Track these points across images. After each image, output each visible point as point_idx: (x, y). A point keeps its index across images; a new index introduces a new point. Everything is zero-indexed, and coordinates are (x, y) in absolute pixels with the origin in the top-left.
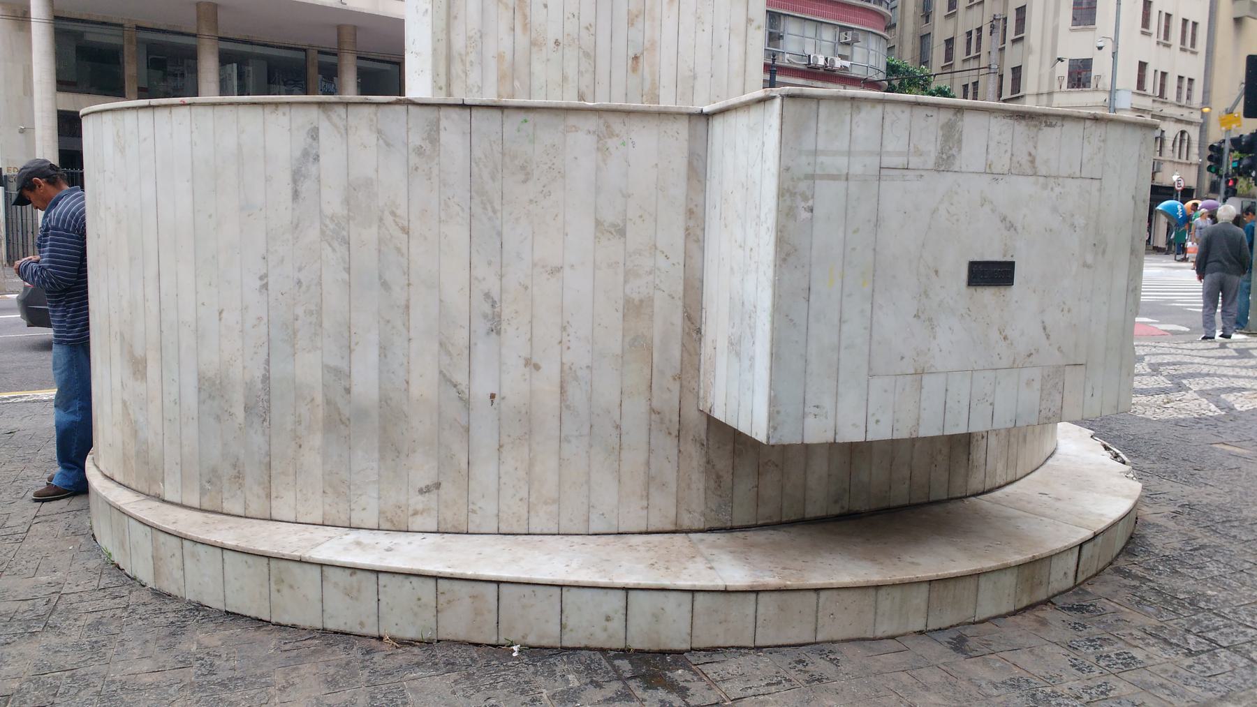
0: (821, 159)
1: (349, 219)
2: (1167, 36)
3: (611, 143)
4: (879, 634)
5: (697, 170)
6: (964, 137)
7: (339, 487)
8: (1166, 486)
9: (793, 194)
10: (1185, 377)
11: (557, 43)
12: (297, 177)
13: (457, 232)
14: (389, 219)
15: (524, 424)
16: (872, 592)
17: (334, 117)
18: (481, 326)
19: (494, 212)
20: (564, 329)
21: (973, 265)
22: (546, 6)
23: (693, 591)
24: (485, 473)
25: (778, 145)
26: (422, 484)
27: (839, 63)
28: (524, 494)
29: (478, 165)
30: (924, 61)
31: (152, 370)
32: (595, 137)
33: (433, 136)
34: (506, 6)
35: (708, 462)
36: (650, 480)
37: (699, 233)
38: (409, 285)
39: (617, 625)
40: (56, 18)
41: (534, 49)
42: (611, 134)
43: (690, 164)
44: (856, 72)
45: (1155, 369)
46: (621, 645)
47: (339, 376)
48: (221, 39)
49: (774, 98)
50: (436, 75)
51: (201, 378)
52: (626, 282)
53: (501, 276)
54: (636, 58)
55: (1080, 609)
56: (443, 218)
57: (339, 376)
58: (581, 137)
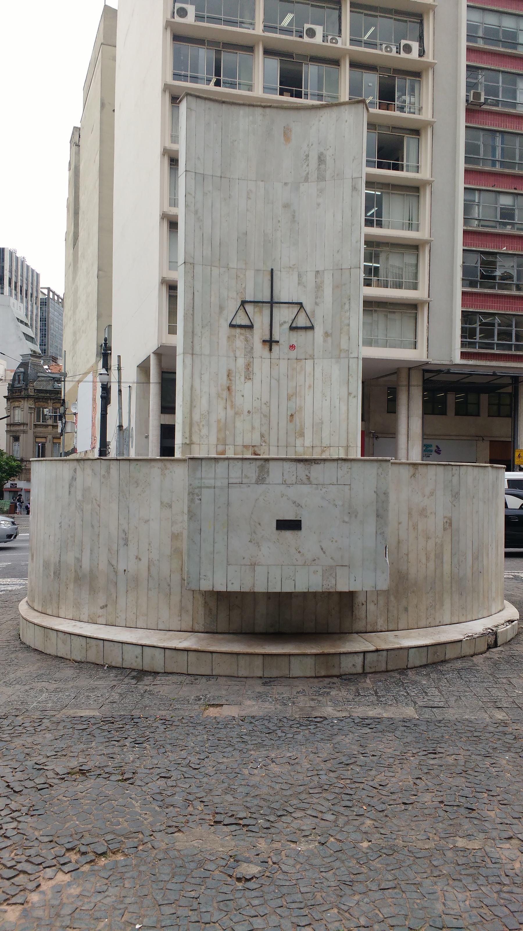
0: (203, 481)
3: (166, 472)
4: (240, 675)
6: (270, 470)
7: (77, 605)
9: (193, 494)
11: (249, 412)
12: (70, 486)
13: (114, 506)
14: (94, 501)
15: (135, 582)
16: (235, 656)
18: (121, 542)
19: (127, 499)
20: (150, 544)
22: (243, 396)
23: (165, 648)
24: (122, 601)
26: (102, 605)
34: (222, 398)
35: (205, 603)
36: (181, 608)
39: (139, 660)
40: (163, 372)
42: (166, 469)
46: (141, 669)
47: (79, 560)
52: (172, 526)
54: (292, 415)
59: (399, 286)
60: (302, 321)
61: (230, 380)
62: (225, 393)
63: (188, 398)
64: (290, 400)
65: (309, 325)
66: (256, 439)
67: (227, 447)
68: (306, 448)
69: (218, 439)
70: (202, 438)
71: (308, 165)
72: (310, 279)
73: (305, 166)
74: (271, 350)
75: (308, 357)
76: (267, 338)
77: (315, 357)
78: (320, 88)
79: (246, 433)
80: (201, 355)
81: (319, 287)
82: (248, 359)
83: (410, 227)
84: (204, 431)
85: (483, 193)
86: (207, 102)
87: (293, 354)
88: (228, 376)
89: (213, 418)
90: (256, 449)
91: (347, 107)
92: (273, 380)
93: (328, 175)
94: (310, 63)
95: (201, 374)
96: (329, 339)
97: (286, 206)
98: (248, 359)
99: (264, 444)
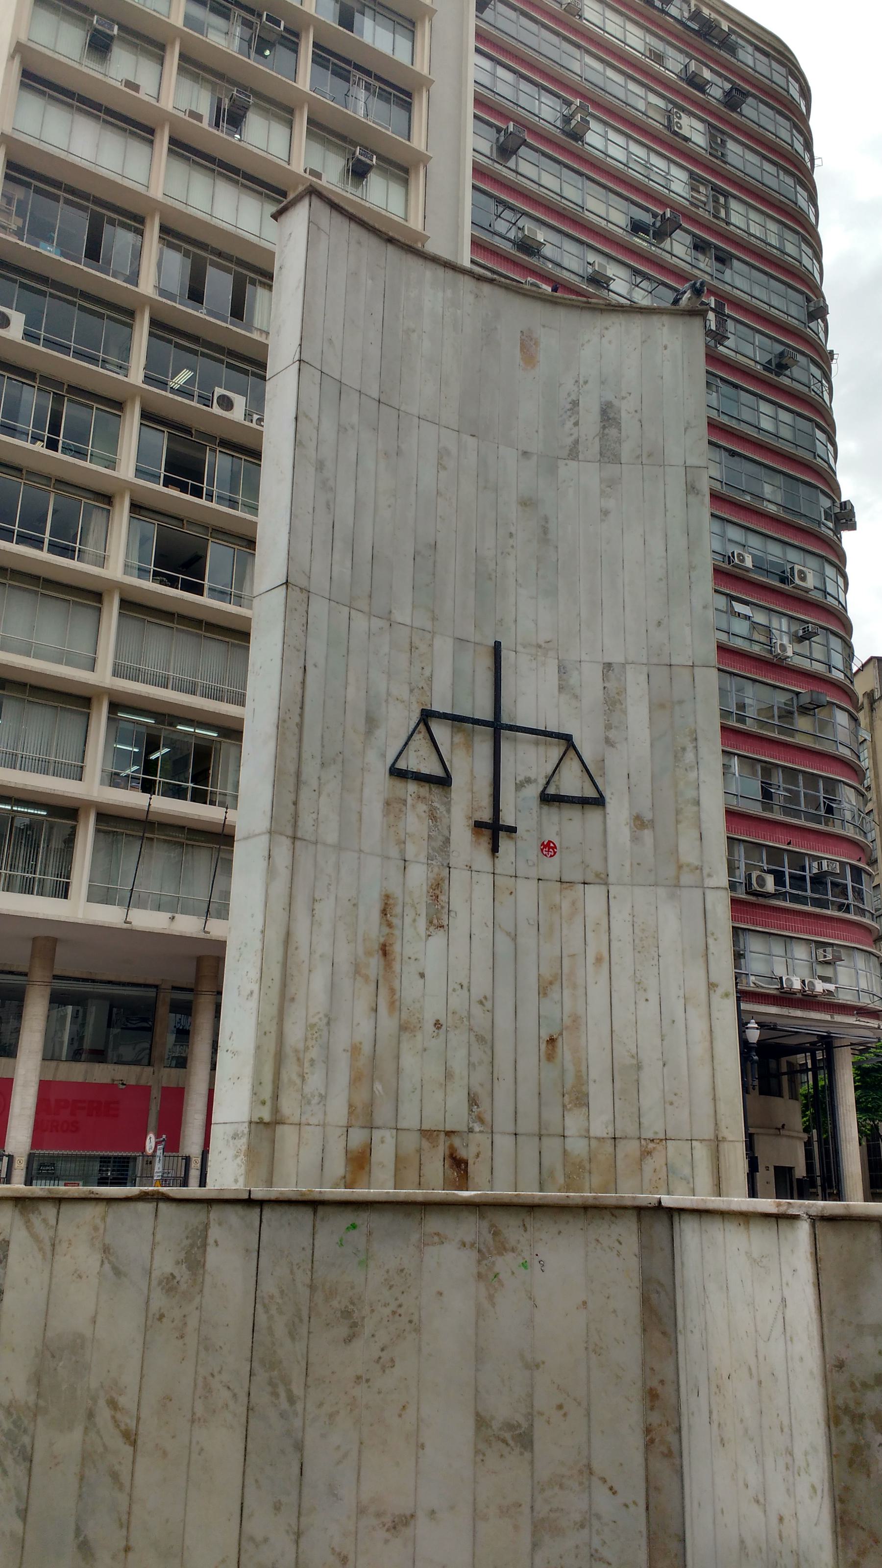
1: (36, 1412)
3: (504, 1264)
5: (659, 1312)
9: (858, 1418)
11: (438, 1025)
13: (221, 1441)
14: (104, 1414)
17: (36, 1221)
19: (292, 1400)
22: (422, 975)
25: (815, 1316)
27: (820, 987)
29: (267, 1310)
32: (474, 1255)
34: (367, 979)
37: (672, 1438)
38: (127, 1549)
41: (405, 1036)
42: (503, 1248)
43: (645, 1301)
44: (845, 998)
48: (55, 977)
49: (796, 1217)
50: (257, 1083)
52: (535, 1546)
53: (298, 1535)
54: (552, 1041)
56: (200, 1411)
60: (571, 782)
61: (390, 925)
62: (375, 963)
63: (275, 971)
64: (545, 994)
65: (590, 793)
66: (457, 1116)
67: (377, 1134)
68: (594, 1143)
69: (350, 1106)
70: (309, 1103)
71: (576, 424)
73: (569, 424)
74: (495, 849)
75: (590, 878)
76: (486, 816)
77: (611, 879)
78: (234, 489)
79: (427, 1092)
80: (316, 843)
81: (613, 703)
82: (436, 870)
84: (315, 1081)
86: (353, 226)
87: (551, 867)
88: (384, 913)
89: (342, 1038)
90: (457, 1142)
91: (665, 319)
92: (501, 937)
93: (626, 451)
94: (219, 449)
95: (315, 900)
96: (647, 835)
97: (527, 503)
98: (436, 870)
99: (477, 1127)
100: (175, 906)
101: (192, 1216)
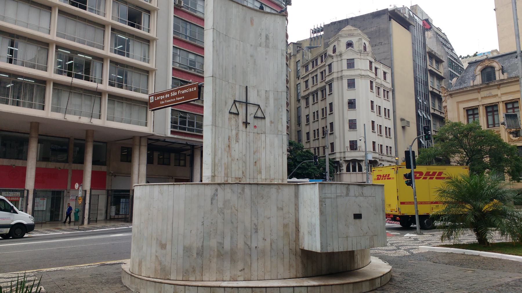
2: (381, 133)
3: (280, 191)
5: (297, 195)
7: (220, 271)
8: (398, 269)
10: (400, 246)
12: (212, 199)
13: (248, 210)
14: (233, 208)
18: (253, 231)
21: (354, 215)
24: (255, 266)
26: (240, 269)
28: (263, 270)
30: (300, 140)
31: (168, 247)
33: (243, 190)
45: (392, 244)
47: (221, 244)
48: (39, 135)
50: (212, 169)
51: (184, 247)
55: (383, 290)
57: (221, 244)
58: (273, 190)
59: (136, 90)
60: (259, 114)
62: (228, 148)
65: (263, 116)
66: (241, 175)
72: (263, 93)
74: (246, 127)
76: (245, 121)
81: (267, 98)
83: (144, 60)
84: (220, 169)
85: (181, 51)
87: (256, 130)
93: (270, 45)
100: (80, 114)
101: (243, 186)
